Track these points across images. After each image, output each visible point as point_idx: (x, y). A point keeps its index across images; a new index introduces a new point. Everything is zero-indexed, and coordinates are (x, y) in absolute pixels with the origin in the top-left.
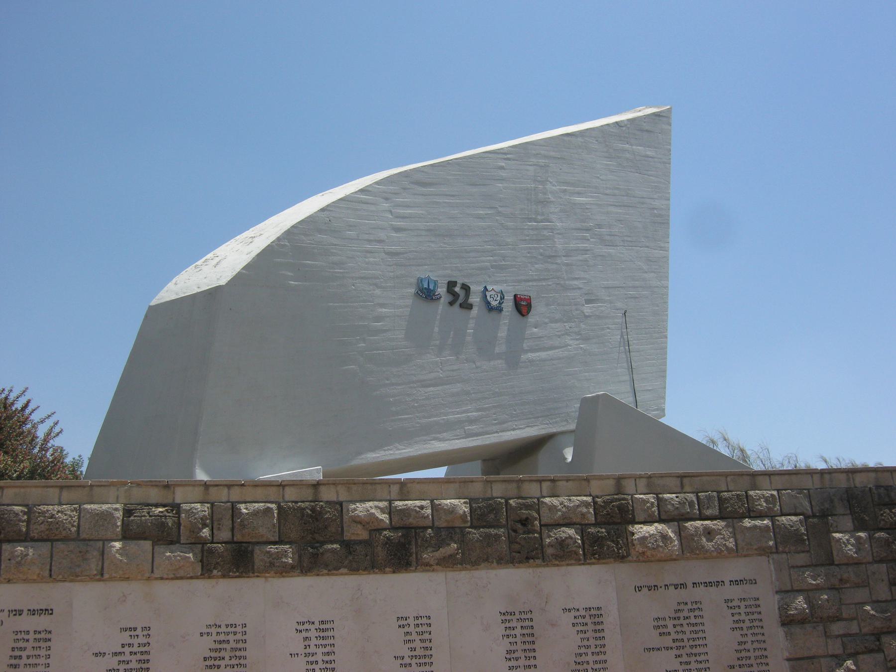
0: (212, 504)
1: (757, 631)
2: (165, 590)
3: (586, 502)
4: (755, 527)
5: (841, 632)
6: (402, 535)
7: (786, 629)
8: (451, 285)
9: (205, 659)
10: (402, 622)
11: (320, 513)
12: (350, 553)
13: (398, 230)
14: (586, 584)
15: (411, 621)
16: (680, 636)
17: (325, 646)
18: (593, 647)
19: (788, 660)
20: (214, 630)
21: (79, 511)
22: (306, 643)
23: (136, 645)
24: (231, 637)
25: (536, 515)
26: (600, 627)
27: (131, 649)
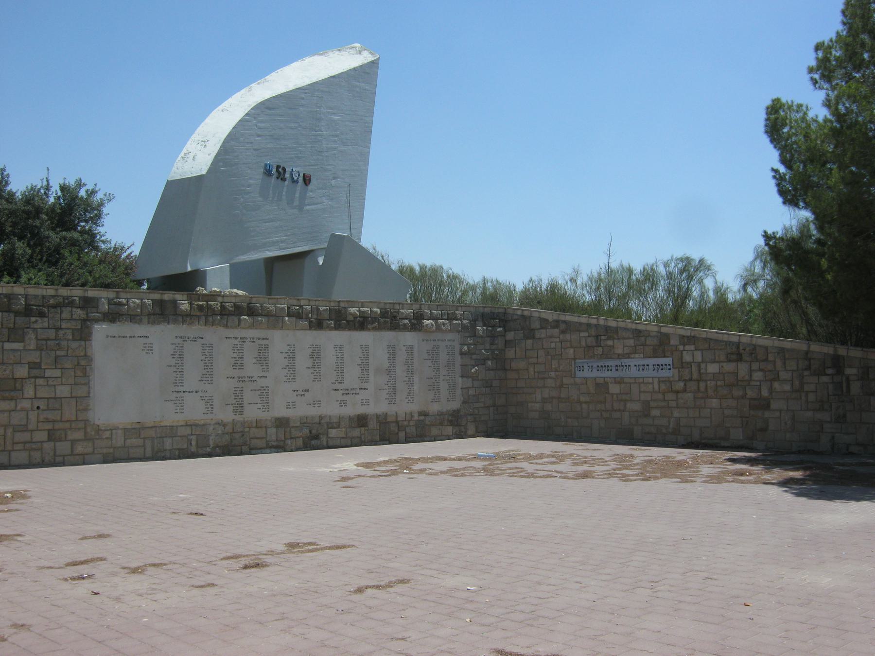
2: (299, 334)
8: (278, 167)
13: (259, 136)
14: (409, 338)
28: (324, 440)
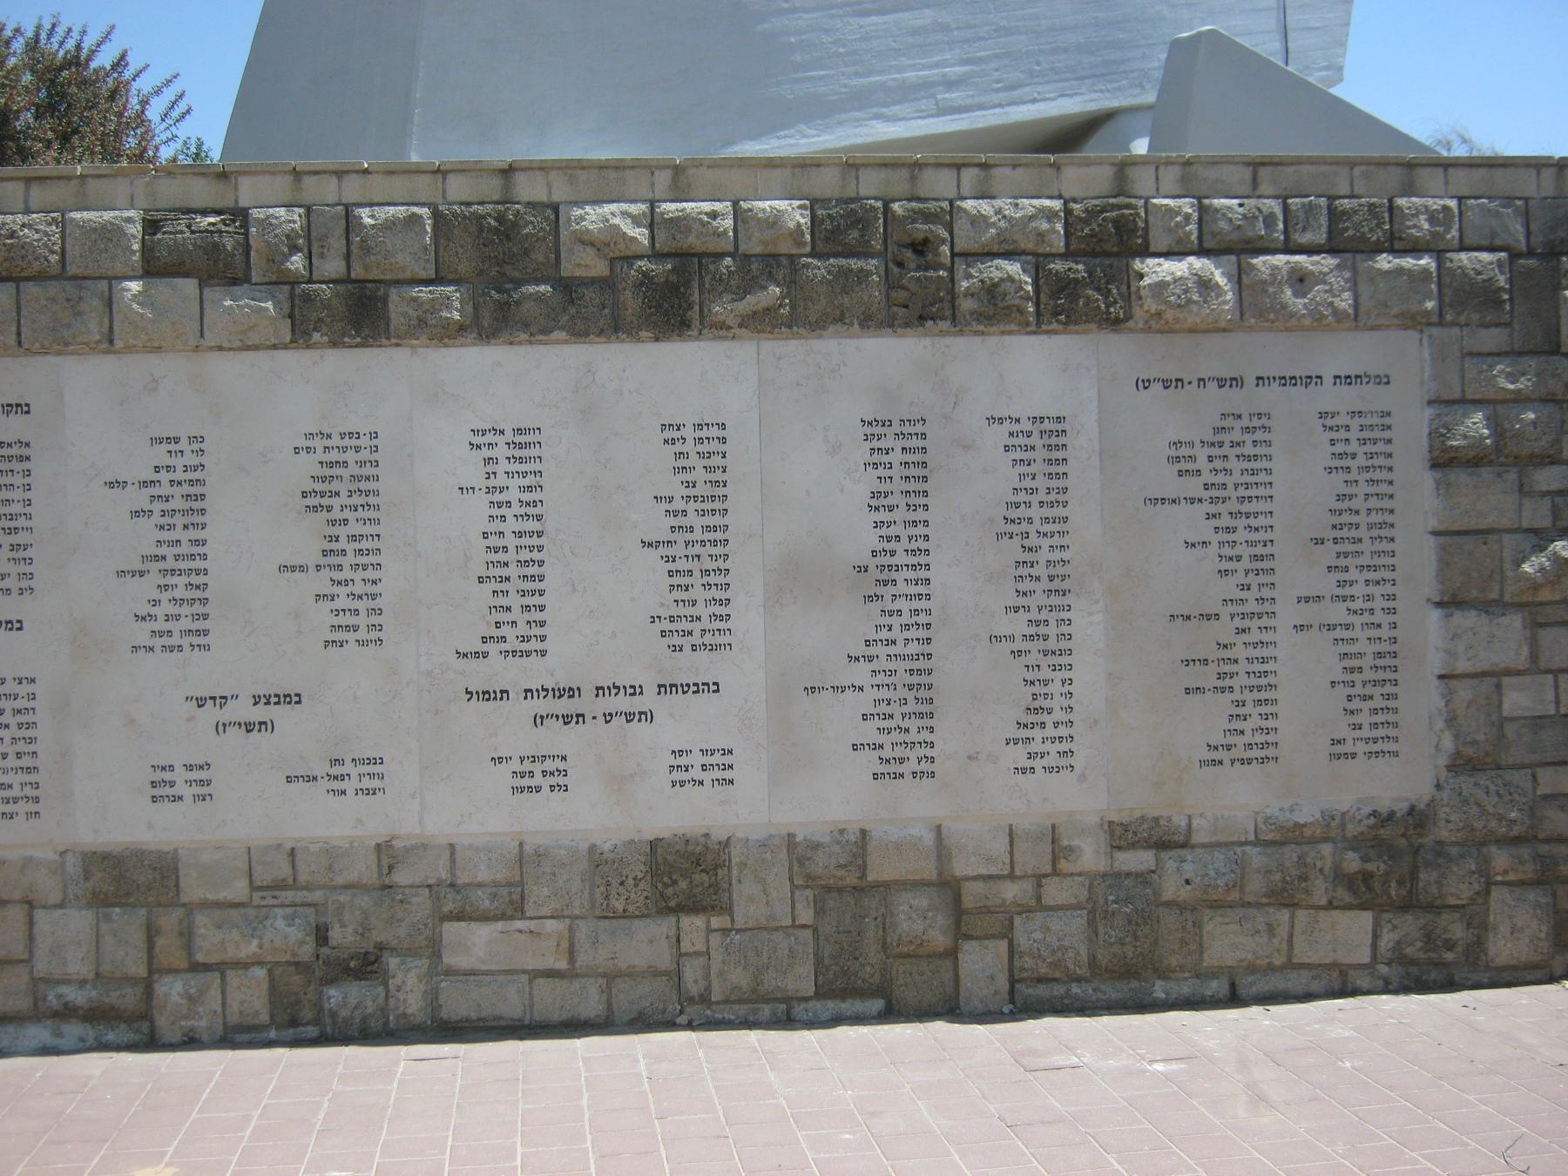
0: (309, 209)
1: (1377, 475)
2: (232, 371)
3: (1050, 210)
4: (1400, 271)
5: (1555, 486)
6: (674, 270)
7: (1439, 475)
9: (304, 495)
10: (669, 434)
11: (515, 225)
12: (572, 302)
14: (1036, 370)
15: (688, 432)
16: (1220, 479)
17: (525, 474)
18: (1042, 491)
19: (1435, 533)
20: (318, 443)
21: (63, 224)
22: (490, 469)
23: (180, 469)
24: (350, 456)
25: (946, 235)
26: (1060, 455)
27: (171, 476)
28: (409, 989)
